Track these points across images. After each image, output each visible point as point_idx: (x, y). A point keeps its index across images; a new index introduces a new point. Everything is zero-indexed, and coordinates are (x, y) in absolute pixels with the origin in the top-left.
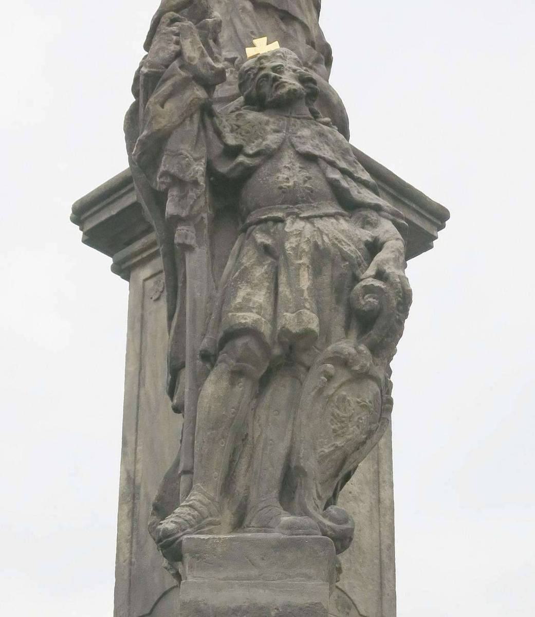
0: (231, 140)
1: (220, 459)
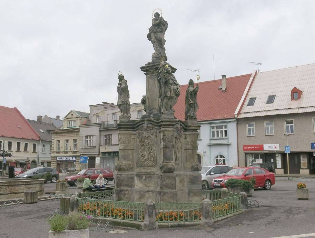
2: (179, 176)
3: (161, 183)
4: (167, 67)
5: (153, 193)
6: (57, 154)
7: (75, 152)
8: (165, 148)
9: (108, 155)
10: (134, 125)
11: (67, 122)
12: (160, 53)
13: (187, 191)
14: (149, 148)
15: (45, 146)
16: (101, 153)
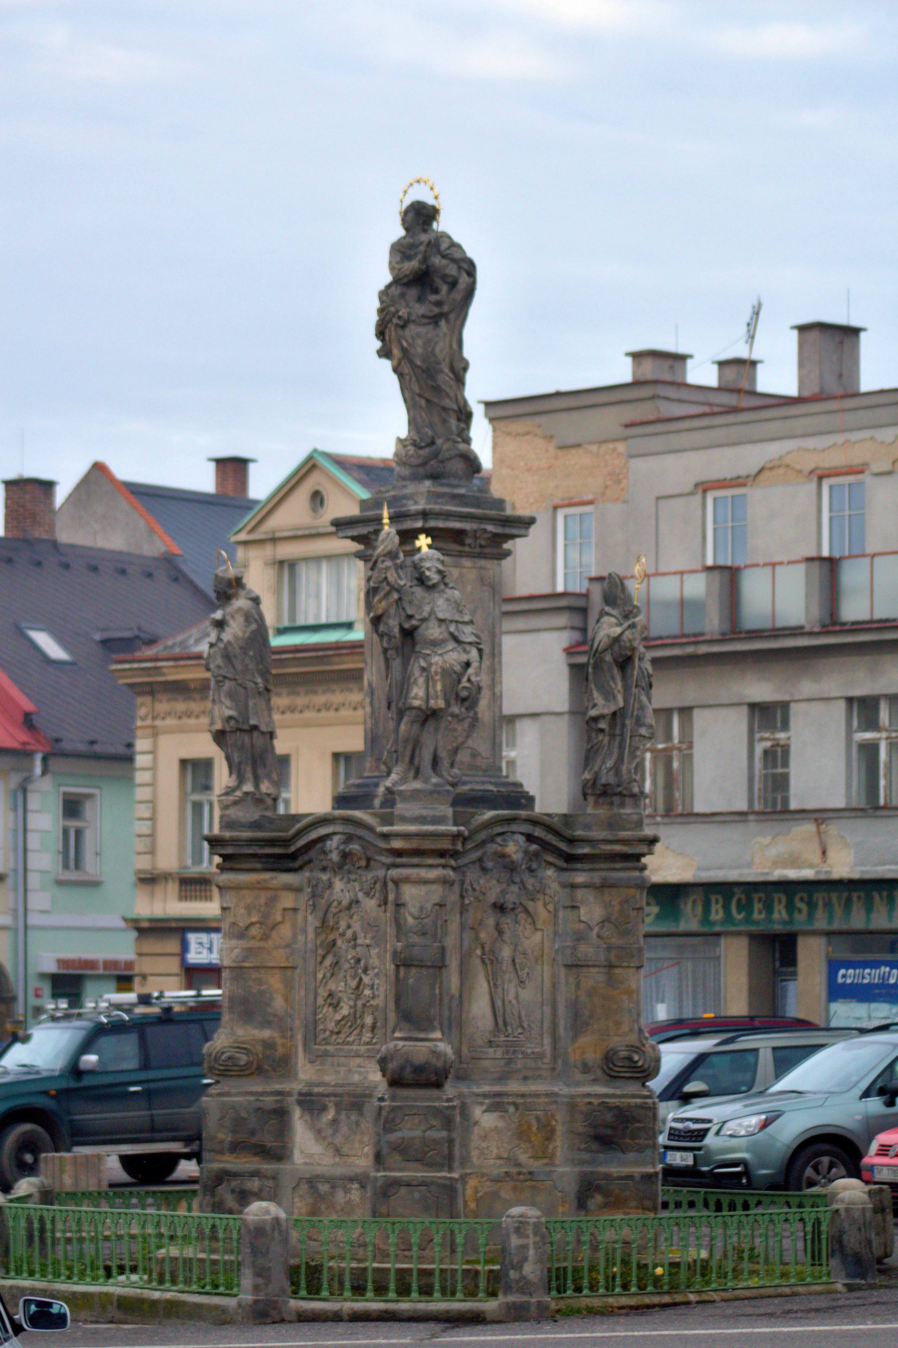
0: (410, 612)
1: (408, 753)
2: (514, 1104)
3: (378, 1134)
4: (425, 549)
6: (183, 897)
8: (402, 969)
9: (659, 917)
10: (286, 842)
12: (429, 441)
13: (571, 1187)
14: (358, 961)
15: (88, 809)
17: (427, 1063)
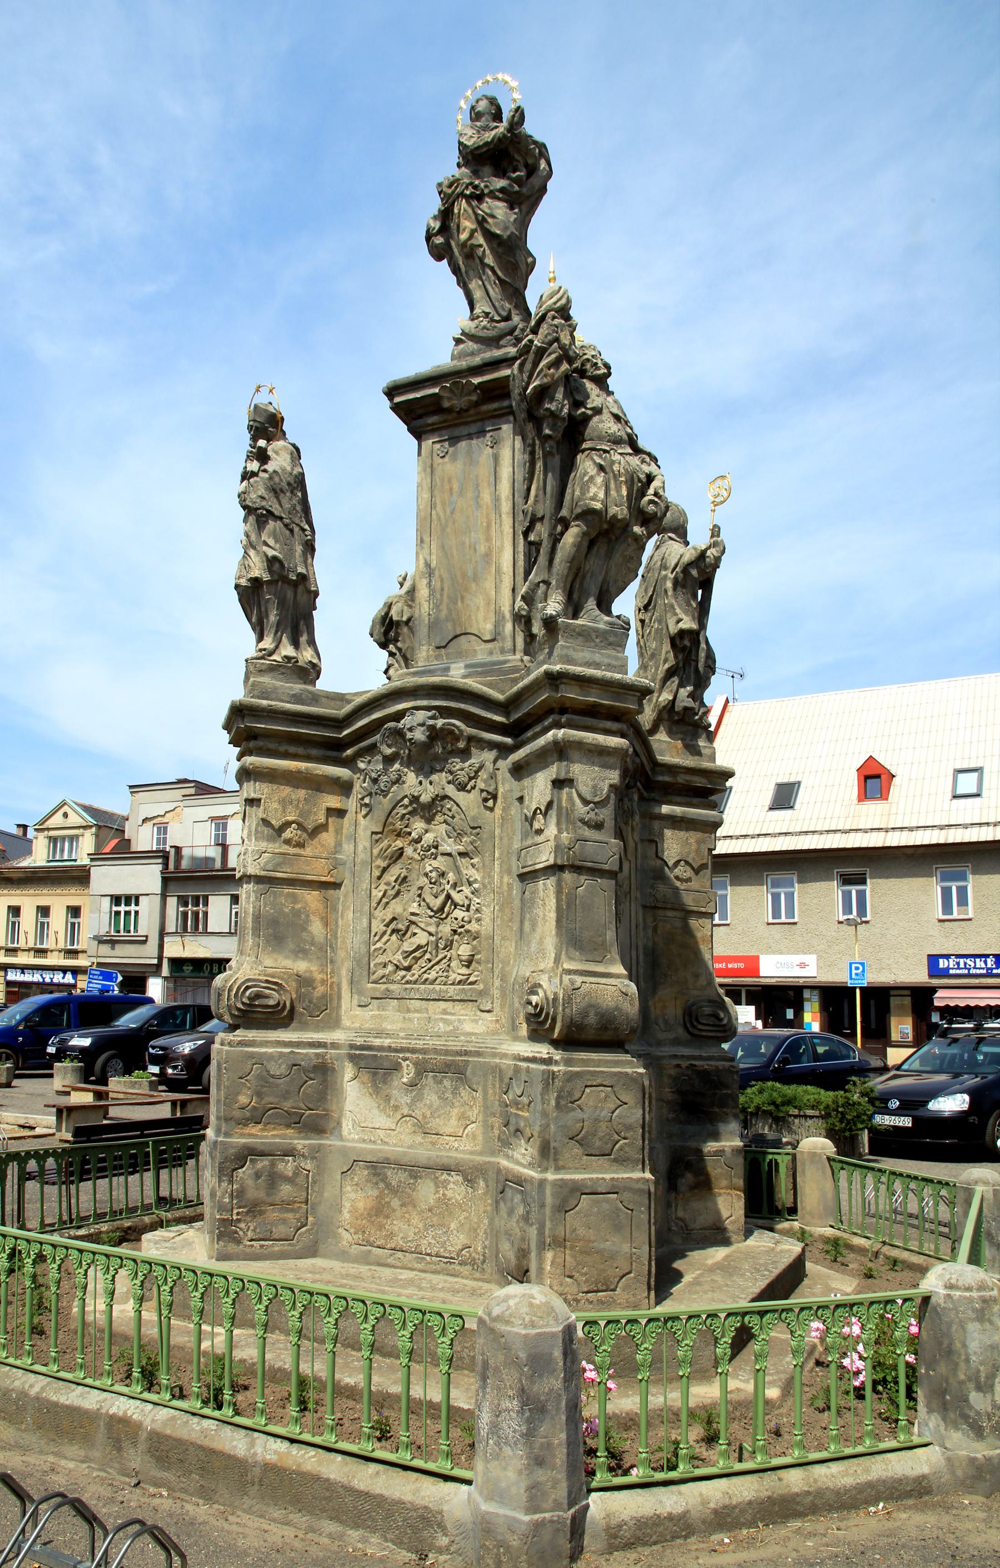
5: (470, 1181)
7: (73, 953)
9: (192, 971)
11: (47, 841)
12: (504, 314)
16: (165, 962)
17: (617, 1008)
